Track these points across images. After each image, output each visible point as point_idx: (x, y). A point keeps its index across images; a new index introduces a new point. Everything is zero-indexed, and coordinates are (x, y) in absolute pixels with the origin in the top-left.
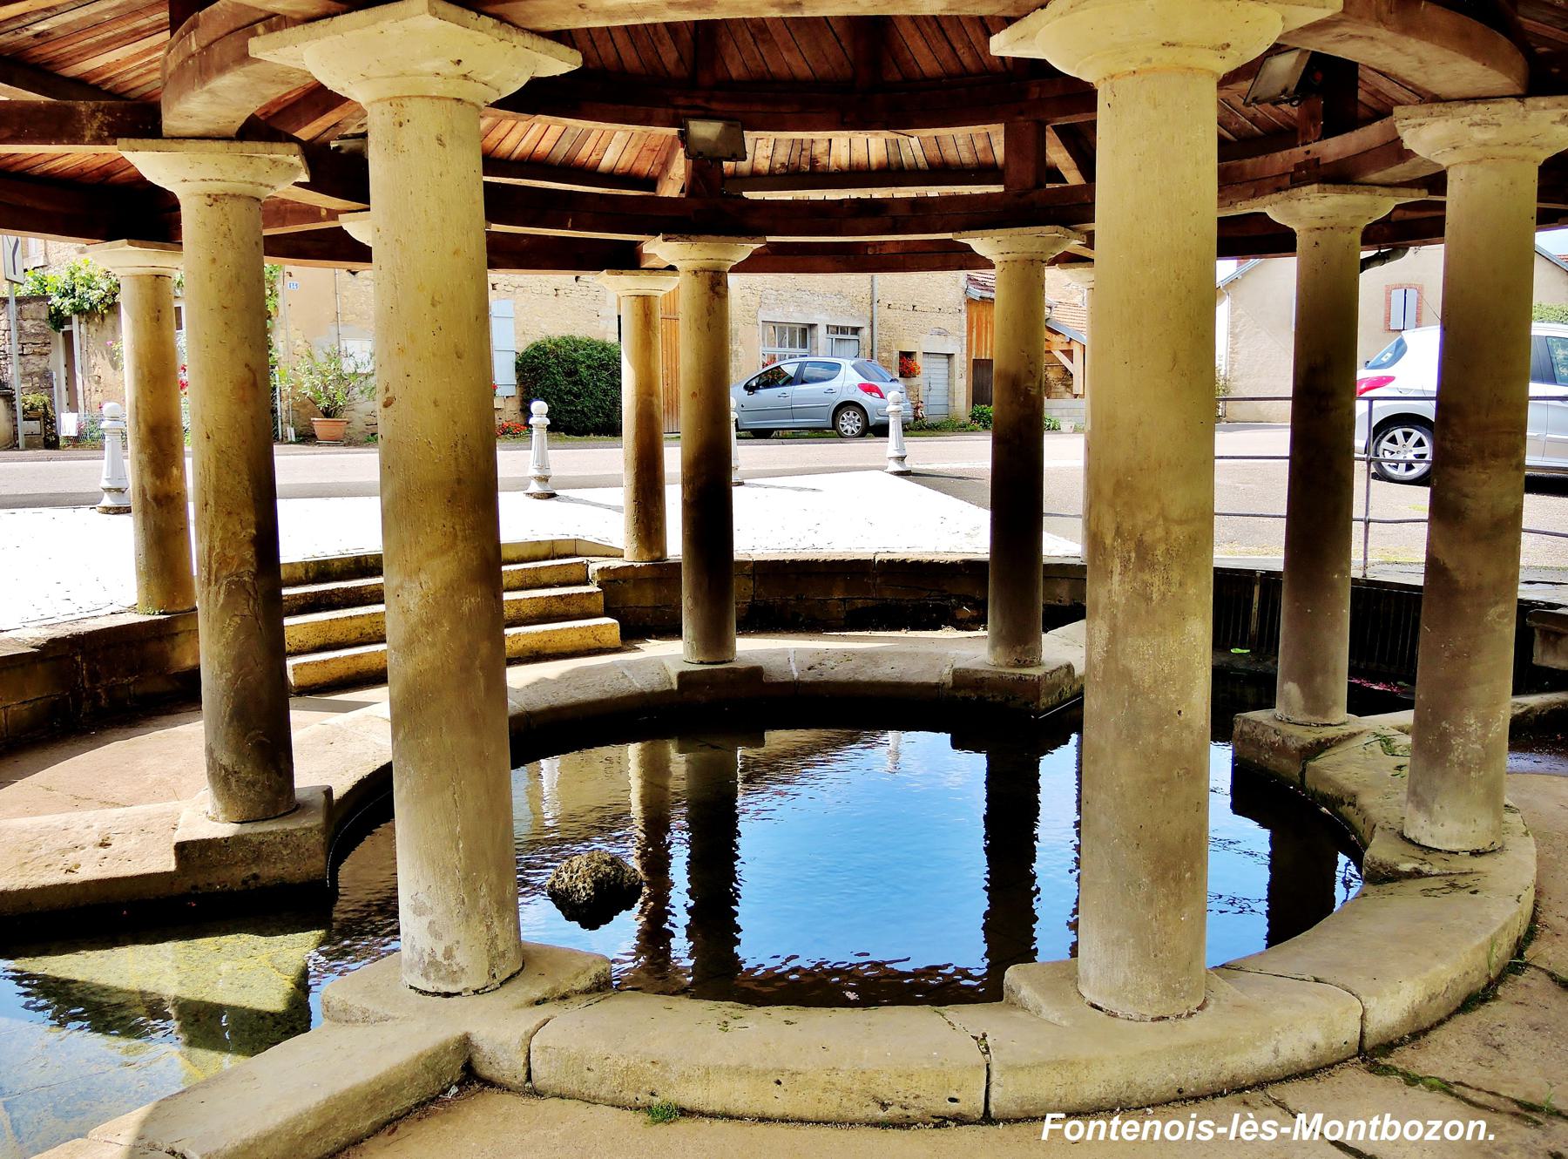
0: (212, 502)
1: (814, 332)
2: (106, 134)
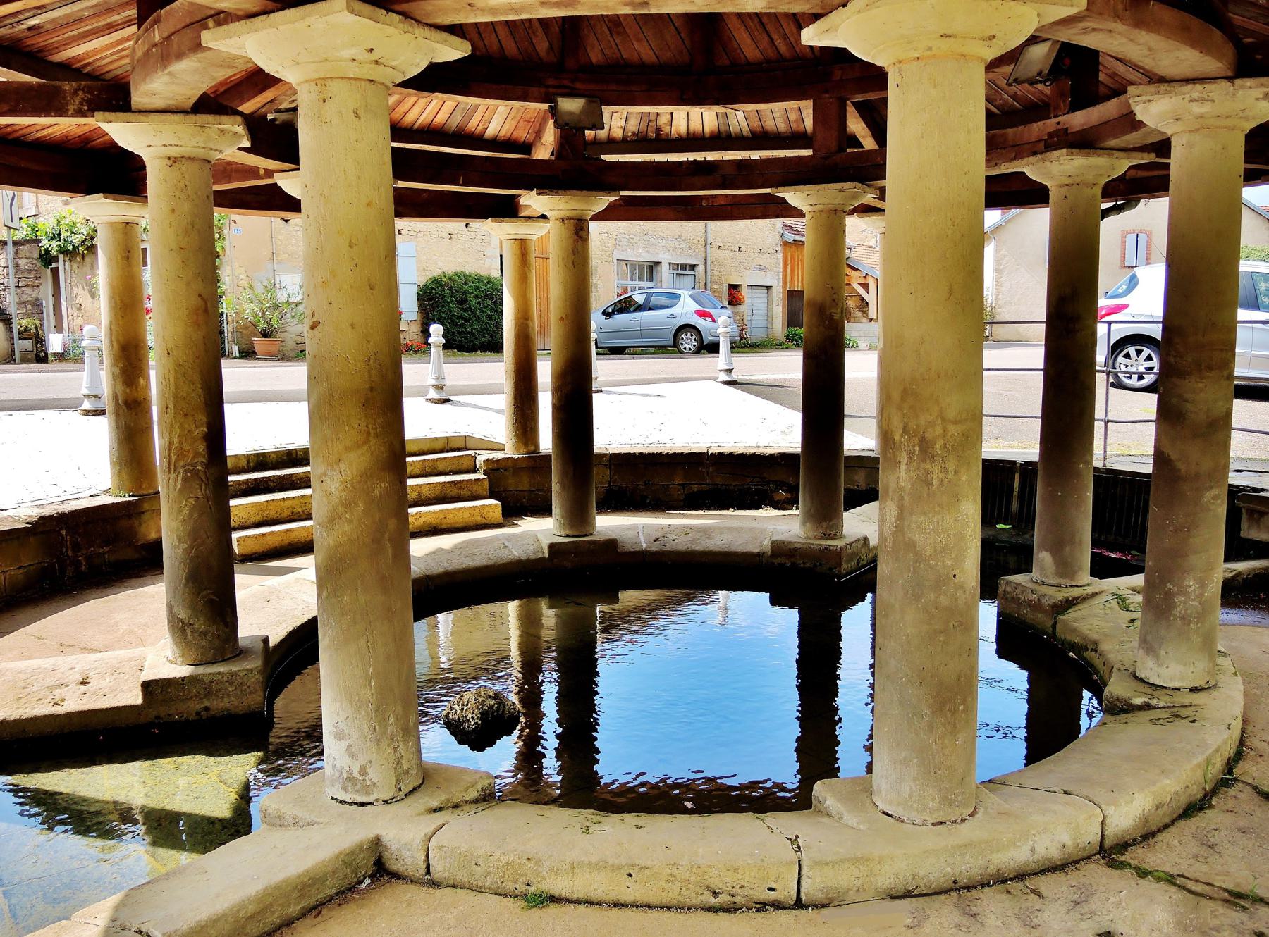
0: (171, 406)
1: (659, 268)
2: (86, 108)
